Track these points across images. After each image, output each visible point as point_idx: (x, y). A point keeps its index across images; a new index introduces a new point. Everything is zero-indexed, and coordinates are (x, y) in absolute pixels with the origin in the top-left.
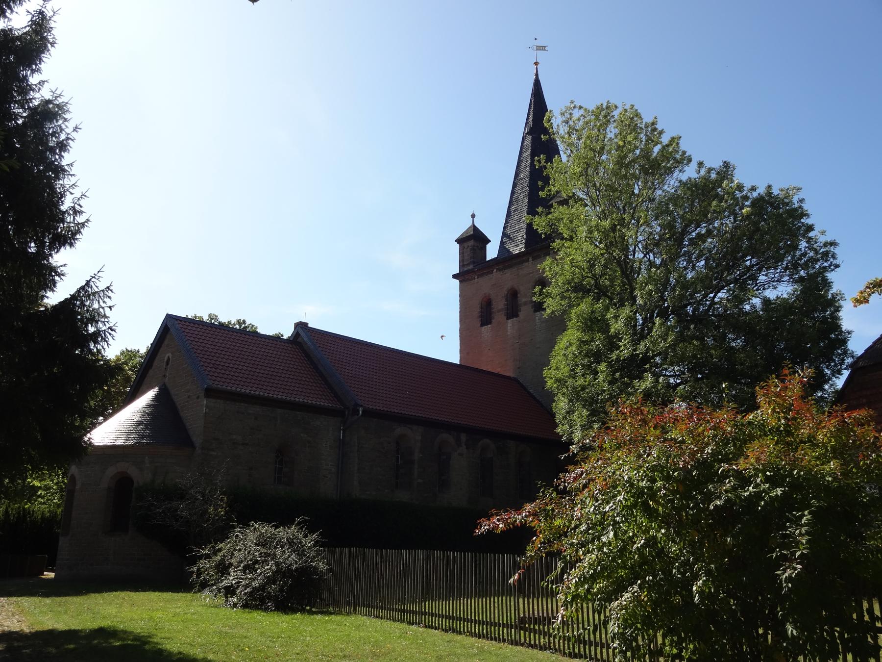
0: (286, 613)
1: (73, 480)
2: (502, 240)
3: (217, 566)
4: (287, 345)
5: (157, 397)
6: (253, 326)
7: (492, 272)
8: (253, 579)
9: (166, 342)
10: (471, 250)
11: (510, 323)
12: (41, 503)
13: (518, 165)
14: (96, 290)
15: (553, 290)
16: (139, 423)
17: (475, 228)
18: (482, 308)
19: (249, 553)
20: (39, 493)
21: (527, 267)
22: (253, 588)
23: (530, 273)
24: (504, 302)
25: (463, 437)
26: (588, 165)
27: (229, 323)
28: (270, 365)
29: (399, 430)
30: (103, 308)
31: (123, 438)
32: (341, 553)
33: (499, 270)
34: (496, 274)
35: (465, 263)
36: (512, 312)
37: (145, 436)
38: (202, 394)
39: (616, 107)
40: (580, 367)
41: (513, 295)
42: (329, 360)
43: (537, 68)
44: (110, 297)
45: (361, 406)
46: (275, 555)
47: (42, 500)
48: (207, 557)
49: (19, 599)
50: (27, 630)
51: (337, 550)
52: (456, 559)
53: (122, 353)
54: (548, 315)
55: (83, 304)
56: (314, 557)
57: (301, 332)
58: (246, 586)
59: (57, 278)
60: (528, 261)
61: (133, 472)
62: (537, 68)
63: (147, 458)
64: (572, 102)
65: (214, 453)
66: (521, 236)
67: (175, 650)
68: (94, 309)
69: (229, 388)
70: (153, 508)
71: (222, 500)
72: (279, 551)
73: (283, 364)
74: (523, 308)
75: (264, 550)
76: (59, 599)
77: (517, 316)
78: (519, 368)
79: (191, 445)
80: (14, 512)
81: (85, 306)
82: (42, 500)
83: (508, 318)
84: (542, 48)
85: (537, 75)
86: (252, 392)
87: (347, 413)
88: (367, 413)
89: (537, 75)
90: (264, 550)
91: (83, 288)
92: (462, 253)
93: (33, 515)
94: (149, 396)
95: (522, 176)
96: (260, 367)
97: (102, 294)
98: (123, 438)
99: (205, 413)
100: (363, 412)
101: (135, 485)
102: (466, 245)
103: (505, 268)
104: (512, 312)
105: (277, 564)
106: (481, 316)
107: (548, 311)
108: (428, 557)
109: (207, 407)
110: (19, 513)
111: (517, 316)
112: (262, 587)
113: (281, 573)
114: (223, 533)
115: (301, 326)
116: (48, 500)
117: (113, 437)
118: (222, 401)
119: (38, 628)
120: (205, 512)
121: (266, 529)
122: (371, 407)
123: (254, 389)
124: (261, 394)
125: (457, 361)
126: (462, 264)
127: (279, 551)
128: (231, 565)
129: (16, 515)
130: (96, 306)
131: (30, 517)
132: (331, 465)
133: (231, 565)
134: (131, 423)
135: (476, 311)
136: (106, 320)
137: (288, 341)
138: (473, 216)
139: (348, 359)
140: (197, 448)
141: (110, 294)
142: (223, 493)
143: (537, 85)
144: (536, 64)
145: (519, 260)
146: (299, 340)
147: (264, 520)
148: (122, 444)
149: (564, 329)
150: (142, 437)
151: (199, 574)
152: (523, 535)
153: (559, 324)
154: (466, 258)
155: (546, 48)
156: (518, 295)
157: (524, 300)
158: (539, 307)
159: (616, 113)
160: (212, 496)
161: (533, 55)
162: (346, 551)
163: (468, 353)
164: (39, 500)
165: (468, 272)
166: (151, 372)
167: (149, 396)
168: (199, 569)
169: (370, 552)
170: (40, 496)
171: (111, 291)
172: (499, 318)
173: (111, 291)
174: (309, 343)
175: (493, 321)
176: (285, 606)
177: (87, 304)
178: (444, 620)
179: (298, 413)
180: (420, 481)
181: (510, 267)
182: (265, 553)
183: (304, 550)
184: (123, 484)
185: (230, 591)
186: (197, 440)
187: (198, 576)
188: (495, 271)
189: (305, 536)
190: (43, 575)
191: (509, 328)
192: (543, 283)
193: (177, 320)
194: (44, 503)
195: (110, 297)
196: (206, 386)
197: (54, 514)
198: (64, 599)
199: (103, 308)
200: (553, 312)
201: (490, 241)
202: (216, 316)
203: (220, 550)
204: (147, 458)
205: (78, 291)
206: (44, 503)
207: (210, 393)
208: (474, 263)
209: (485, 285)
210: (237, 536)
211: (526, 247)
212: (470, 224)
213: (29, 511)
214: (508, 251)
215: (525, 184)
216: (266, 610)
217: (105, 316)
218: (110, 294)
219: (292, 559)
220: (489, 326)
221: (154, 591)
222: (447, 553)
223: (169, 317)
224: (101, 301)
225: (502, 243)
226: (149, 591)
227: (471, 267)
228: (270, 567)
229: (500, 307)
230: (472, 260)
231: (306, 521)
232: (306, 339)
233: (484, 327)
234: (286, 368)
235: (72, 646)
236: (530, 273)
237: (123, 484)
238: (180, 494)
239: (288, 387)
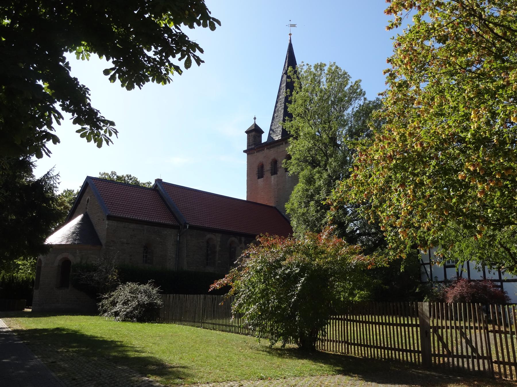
0: (141, 323)
1: (40, 261)
2: (269, 132)
3: (111, 303)
4: (151, 191)
5: (83, 220)
6: (135, 178)
7: (264, 150)
8: (127, 308)
9: (87, 190)
10: (253, 137)
12: (21, 273)
13: (279, 91)
14: (52, 176)
15: (293, 161)
16: (73, 233)
17: (255, 125)
18: (258, 169)
19: (126, 296)
21: (282, 147)
22: (127, 312)
24: (270, 166)
25: (243, 239)
26: (306, 101)
27: (123, 176)
28: (141, 203)
29: (209, 236)
30: (55, 184)
32: (170, 296)
33: (268, 148)
34: (266, 151)
36: (274, 171)
37: (77, 240)
38: (106, 218)
39: (325, 65)
40: (303, 203)
41: (275, 163)
42: (173, 199)
43: (290, 37)
44: (58, 179)
45: (188, 224)
46: (138, 297)
47: (22, 271)
48: (107, 298)
49: (17, 318)
50: (24, 329)
51: (168, 295)
53: (65, 191)
54: (291, 175)
55: (46, 183)
56: (156, 298)
57: (158, 184)
58: (125, 311)
59: (33, 167)
60: (282, 144)
61: (71, 257)
62: (290, 37)
64: (303, 62)
65: (112, 248)
66: (279, 130)
67: (89, 335)
68: (51, 184)
69: (119, 215)
70: (81, 276)
71: (115, 272)
72: (139, 296)
73: (148, 202)
75: (132, 295)
76: (36, 319)
77: (276, 174)
79: (101, 244)
80: (7, 277)
81: (47, 183)
82: (22, 271)
83: (272, 175)
84: (294, 26)
85: (290, 41)
86: (132, 217)
88: (191, 227)
89: (290, 41)
90: (132, 295)
91: (46, 175)
94: (78, 219)
95: (281, 97)
96: (136, 204)
97: (55, 178)
100: (189, 227)
101: (72, 264)
102: (250, 134)
105: (138, 301)
106: (258, 173)
107: (291, 172)
108: (205, 298)
109: (108, 225)
110: (10, 278)
111: (276, 174)
112: (131, 312)
113: (140, 305)
114: (114, 288)
115: (158, 181)
117: (60, 240)
119: (28, 328)
120: (107, 277)
121: (134, 286)
122: (193, 224)
123: (133, 215)
124: (136, 218)
125: (245, 199)
127: (139, 296)
128: (117, 302)
129: (9, 279)
130: (52, 183)
131: (16, 280)
133: (117, 302)
134: (69, 233)
135: (256, 170)
136: (57, 189)
137: (151, 189)
138: (255, 118)
139: (183, 198)
141: (58, 177)
142: (116, 268)
143: (290, 46)
144: (290, 34)
146: (157, 189)
147: (133, 281)
149: (297, 182)
150: (75, 240)
151: (103, 307)
152: (226, 288)
153: (295, 179)
155: (296, 26)
158: (286, 170)
159: (326, 68)
160: (110, 270)
162: (172, 295)
163: (251, 193)
164: (20, 271)
165: (252, 149)
166: (79, 206)
167: (78, 219)
168: (102, 304)
169: (182, 296)
170: (21, 269)
172: (267, 174)
174: (162, 190)
175: (264, 176)
176: (141, 320)
177: (48, 182)
181: (273, 147)
182: (133, 296)
183: (151, 295)
184: (66, 264)
185: (116, 314)
186: (103, 242)
187: (102, 307)
188: (266, 149)
189: (153, 289)
192: (289, 157)
193: (92, 179)
194: (23, 273)
195: (58, 179)
197: (28, 279)
198: (39, 318)
199: (55, 184)
200: (294, 173)
202: (115, 172)
203: (113, 295)
205: (44, 177)
206: (23, 273)
207: (109, 218)
208: (255, 144)
209: (260, 156)
210: (120, 289)
211: (282, 137)
212: (253, 123)
213: (15, 277)
214: (273, 138)
215: (282, 102)
216: (133, 322)
217: (56, 187)
218: (58, 177)
219: (145, 299)
221: (82, 315)
223: (88, 178)
224: (54, 181)
225: (270, 134)
226: (79, 315)
227: (253, 146)
228: (135, 303)
231: (152, 282)
232: (160, 188)
234: (150, 204)
235: (46, 333)
237: (66, 264)
238: (95, 269)
239: (150, 214)
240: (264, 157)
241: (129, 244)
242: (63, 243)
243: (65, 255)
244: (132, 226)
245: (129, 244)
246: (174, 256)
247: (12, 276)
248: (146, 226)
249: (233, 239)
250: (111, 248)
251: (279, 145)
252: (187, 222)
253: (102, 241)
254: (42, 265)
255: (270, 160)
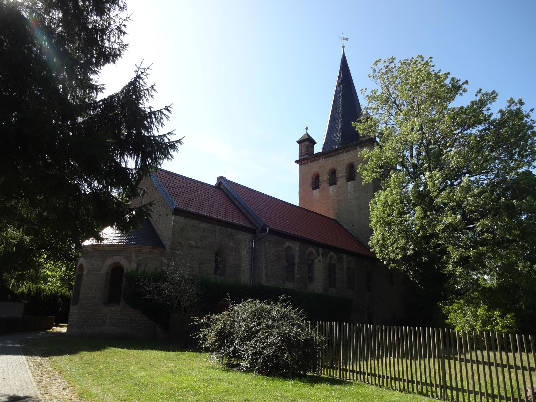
10: (306, 147)
11: (331, 188)
12: (49, 285)
18: (313, 180)
20: (49, 279)
23: (344, 160)
25: (321, 250)
29: (288, 244)
31: (117, 240)
33: (324, 158)
34: (322, 161)
35: (302, 154)
38: (171, 213)
43: (344, 49)
45: (268, 226)
48: (208, 326)
52: (333, 327)
57: (223, 182)
60: (343, 153)
61: (124, 263)
62: (344, 49)
63: (133, 253)
65: (178, 253)
74: (339, 180)
77: (336, 184)
78: (337, 214)
79: (163, 246)
83: (330, 186)
84: (346, 39)
85: (344, 53)
87: (257, 231)
88: (272, 232)
89: (344, 53)
92: (300, 149)
93: (45, 292)
98: (117, 240)
99: (173, 225)
100: (269, 230)
101: (125, 271)
102: (303, 144)
103: (328, 157)
104: (333, 181)
106: (313, 184)
109: (174, 221)
110: (37, 290)
111: (336, 184)
115: (221, 180)
116: (53, 284)
118: (184, 218)
126: (300, 155)
131: (43, 293)
132: (247, 264)
138: (307, 129)
140: (167, 249)
141: (153, 93)
143: (344, 58)
144: (343, 47)
145: (337, 152)
146: (222, 187)
148: (117, 243)
154: (303, 151)
155: (348, 40)
156: (337, 172)
157: (340, 175)
161: (342, 42)
165: (305, 159)
170: (49, 282)
171: (155, 90)
172: (324, 185)
173: (155, 90)
174: (229, 188)
175: (320, 187)
178: (335, 371)
179: (228, 229)
180: (298, 276)
181: (331, 156)
186: (167, 243)
188: (321, 158)
190: (52, 329)
191: (330, 191)
196: (174, 207)
201: (316, 143)
204: (133, 253)
206: (51, 286)
207: (177, 212)
208: (308, 154)
209: (314, 167)
212: (305, 133)
213: (43, 290)
218: (153, 93)
220: (318, 190)
222: (349, 325)
227: (306, 156)
229: (325, 179)
230: (307, 152)
233: (331, 187)
236: (344, 160)
240: (320, 167)
241: (198, 248)
242: (114, 243)
243: (117, 259)
244: (203, 225)
245: (198, 248)
246: (248, 267)
247: (40, 287)
248: (218, 227)
249: (311, 249)
250: (177, 252)
251: (339, 154)
252: (267, 224)
253: (164, 242)
254: (85, 272)
255: (328, 170)
